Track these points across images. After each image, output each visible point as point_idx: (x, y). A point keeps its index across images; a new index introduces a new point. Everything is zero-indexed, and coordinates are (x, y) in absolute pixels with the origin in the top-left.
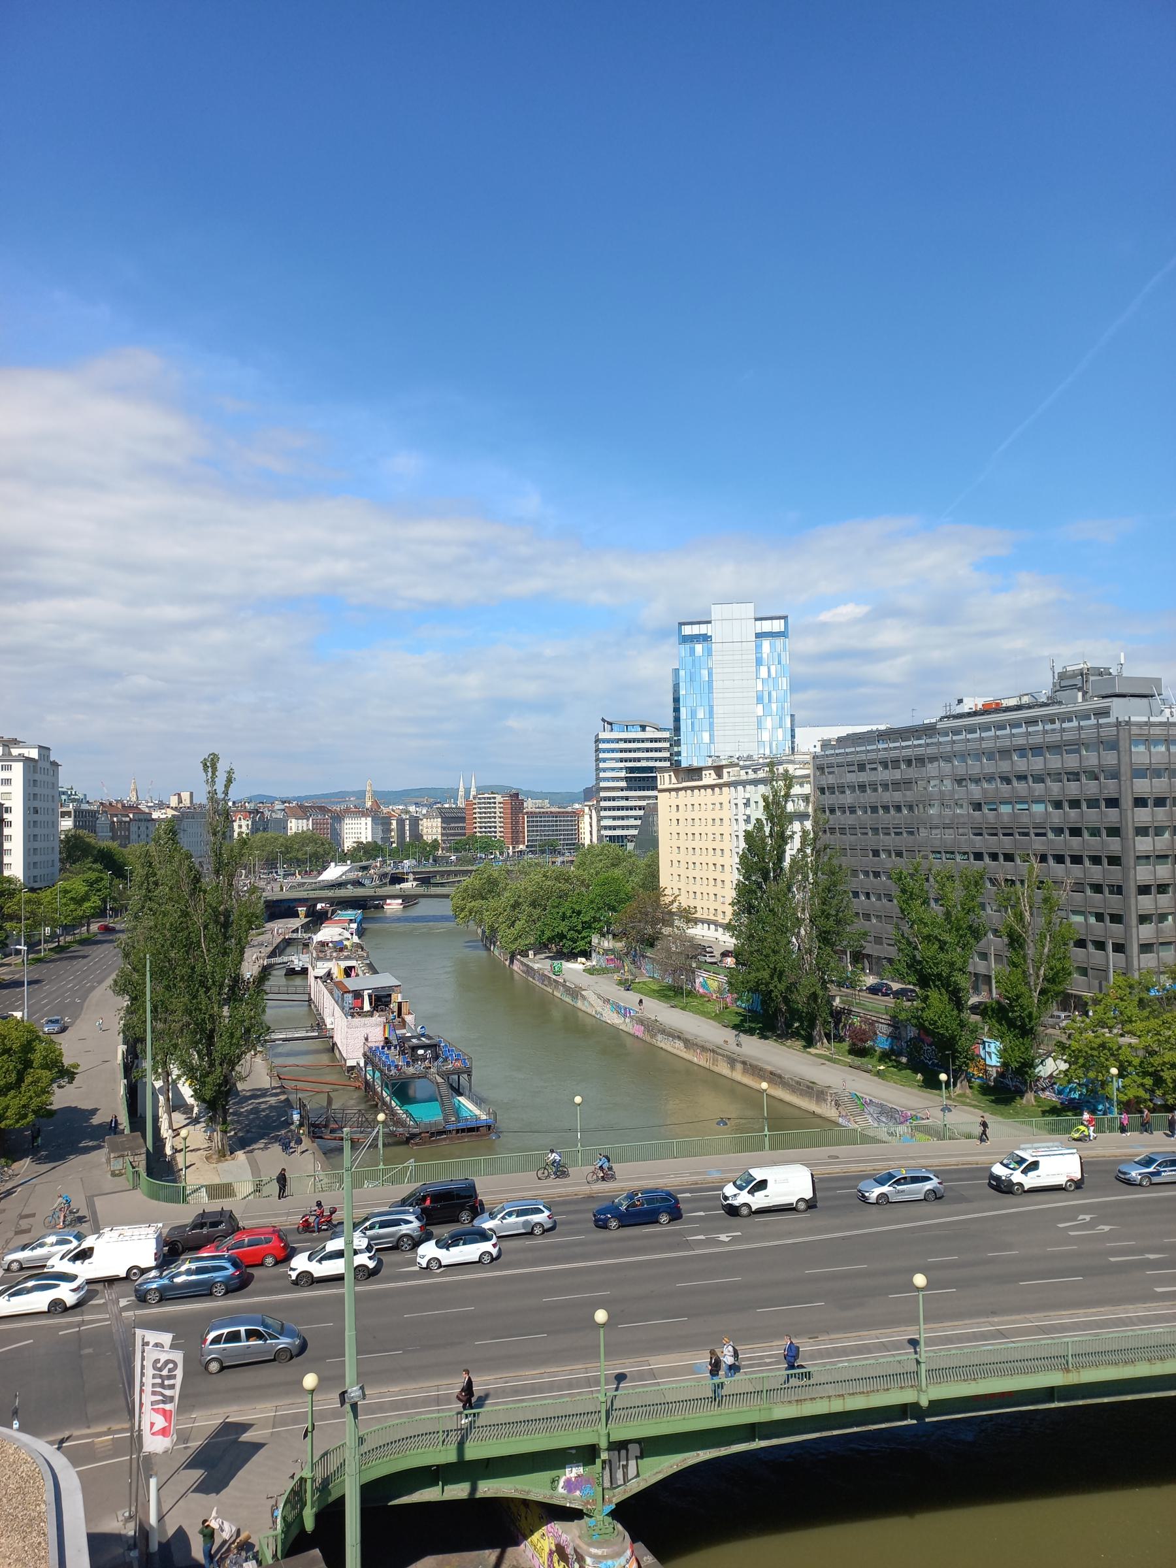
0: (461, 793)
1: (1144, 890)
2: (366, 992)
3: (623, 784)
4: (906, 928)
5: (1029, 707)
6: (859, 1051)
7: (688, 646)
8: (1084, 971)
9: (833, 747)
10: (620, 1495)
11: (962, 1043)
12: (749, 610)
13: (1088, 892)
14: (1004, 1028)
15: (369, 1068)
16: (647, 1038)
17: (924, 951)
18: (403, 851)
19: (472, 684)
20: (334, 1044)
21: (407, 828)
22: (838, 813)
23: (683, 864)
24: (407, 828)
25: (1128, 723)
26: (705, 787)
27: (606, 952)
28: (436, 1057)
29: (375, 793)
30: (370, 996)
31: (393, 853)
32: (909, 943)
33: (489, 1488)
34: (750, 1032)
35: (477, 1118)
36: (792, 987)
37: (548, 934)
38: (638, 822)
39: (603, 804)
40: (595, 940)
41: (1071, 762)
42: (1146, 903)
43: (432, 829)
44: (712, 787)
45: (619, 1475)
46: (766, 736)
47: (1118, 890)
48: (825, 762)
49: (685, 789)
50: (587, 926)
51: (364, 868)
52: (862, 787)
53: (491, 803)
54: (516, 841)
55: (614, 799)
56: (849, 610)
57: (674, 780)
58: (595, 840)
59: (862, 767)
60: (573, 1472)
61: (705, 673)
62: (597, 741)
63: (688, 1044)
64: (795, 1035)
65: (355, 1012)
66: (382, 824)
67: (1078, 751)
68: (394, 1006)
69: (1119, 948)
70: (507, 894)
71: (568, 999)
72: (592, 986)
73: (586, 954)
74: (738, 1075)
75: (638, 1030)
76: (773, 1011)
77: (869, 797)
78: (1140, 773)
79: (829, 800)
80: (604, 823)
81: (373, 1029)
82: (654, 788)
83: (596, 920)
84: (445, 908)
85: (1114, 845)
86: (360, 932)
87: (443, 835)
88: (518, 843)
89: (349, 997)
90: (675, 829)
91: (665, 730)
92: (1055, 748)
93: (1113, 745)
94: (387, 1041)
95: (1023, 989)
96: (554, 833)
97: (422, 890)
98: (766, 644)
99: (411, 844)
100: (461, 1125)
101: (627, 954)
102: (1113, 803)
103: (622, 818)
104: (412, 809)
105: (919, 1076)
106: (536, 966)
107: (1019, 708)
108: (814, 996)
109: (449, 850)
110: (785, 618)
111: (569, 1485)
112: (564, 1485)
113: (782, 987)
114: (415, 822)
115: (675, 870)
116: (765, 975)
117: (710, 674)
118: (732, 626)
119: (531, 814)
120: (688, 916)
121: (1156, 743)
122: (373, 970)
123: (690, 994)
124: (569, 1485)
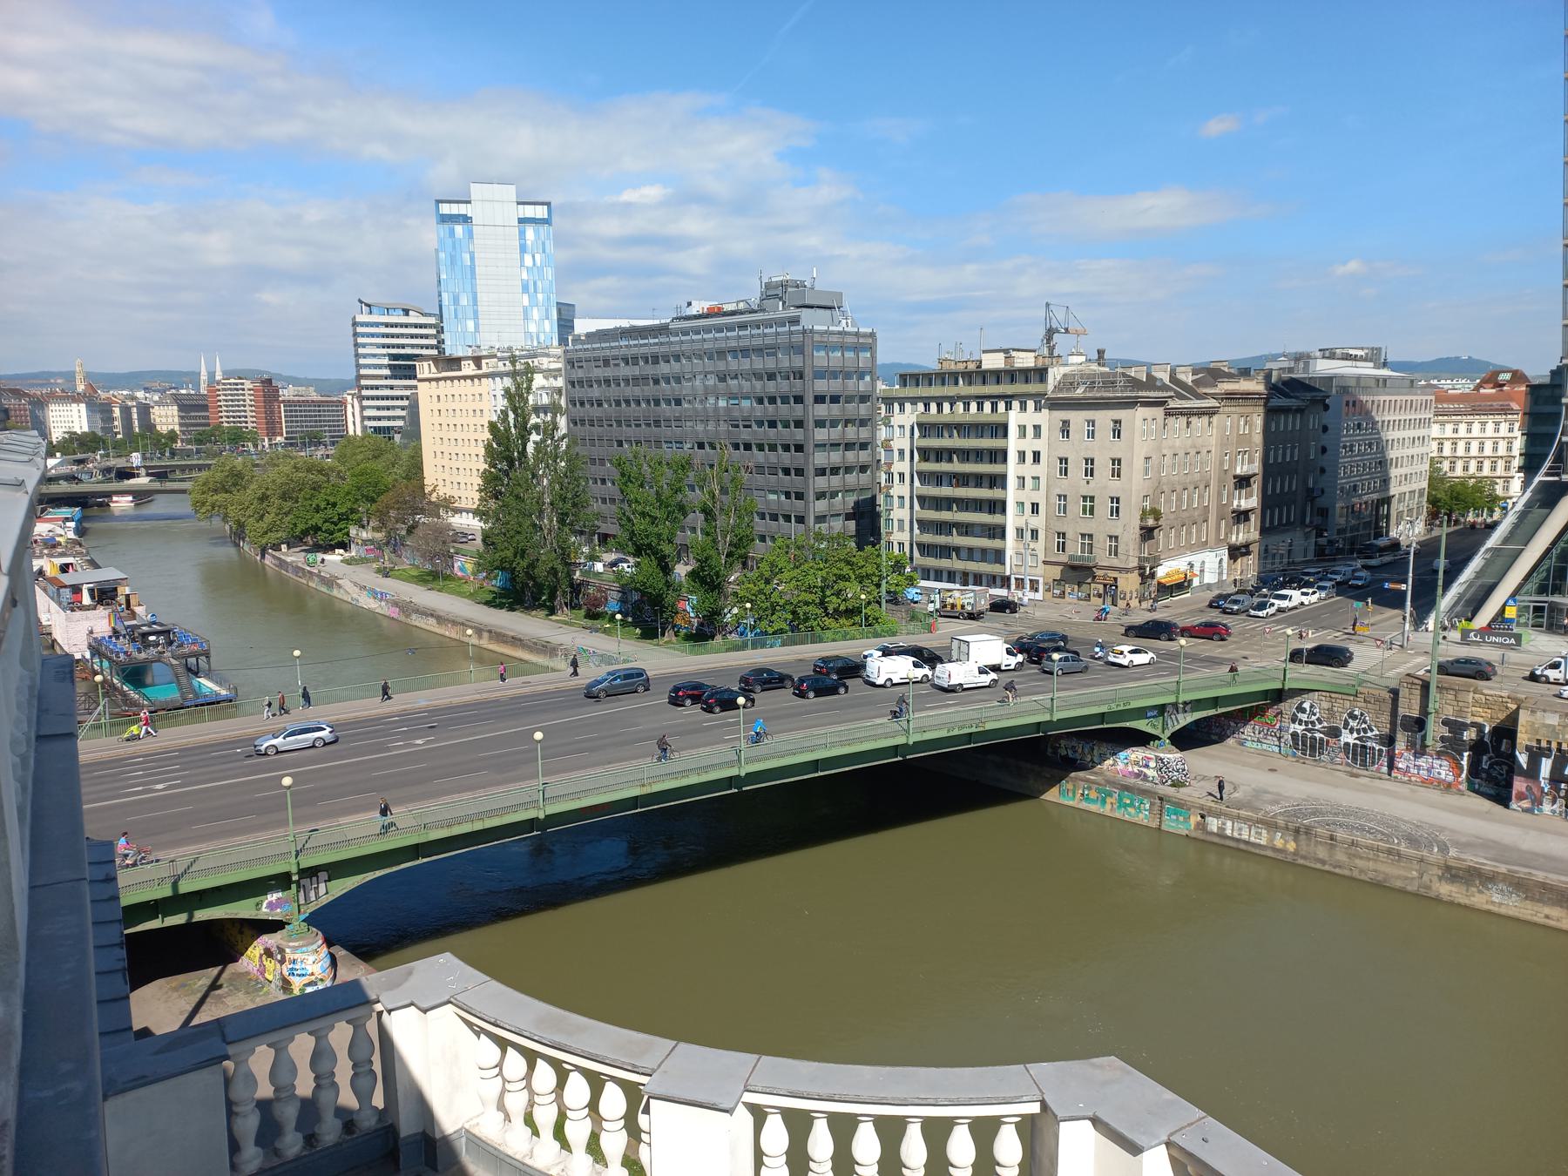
0: (204, 377)
1: (821, 472)
2: (85, 587)
3: (387, 372)
4: (626, 506)
5: (741, 313)
6: (592, 616)
7: (446, 226)
8: (763, 539)
9: (583, 343)
10: (312, 908)
11: (669, 599)
12: (510, 192)
13: (781, 475)
14: (697, 585)
15: (96, 660)
16: (402, 618)
17: (640, 525)
18: (131, 442)
19: (217, 248)
20: (54, 641)
21: (135, 416)
22: (664, 405)
23: (446, 455)
24: (135, 416)
25: (812, 331)
26: (465, 378)
27: (365, 542)
28: (170, 643)
29: (88, 376)
30: (91, 591)
31: (117, 445)
32: (629, 520)
33: (201, 915)
34: (500, 606)
35: (217, 694)
36: (532, 565)
37: (301, 527)
38: (403, 413)
39: (365, 393)
40: (353, 531)
41: (770, 363)
42: (821, 483)
43: (166, 418)
44: (472, 378)
45: (312, 894)
46: (533, 328)
47: (800, 472)
48: (575, 356)
49: (445, 379)
50: (344, 518)
51: (80, 462)
52: (607, 381)
53: (237, 388)
54: (272, 431)
55: (377, 388)
56: (652, 193)
57: (434, 369)
58: (359, 433)
59: (606, 362)
60: (273, 897)
61: (467, 257)
62: (355, 324)
63: (440, 619)
64: (542, 606)
65: (75, 606)
66: (102, 412)
67: (775, 354)
68: (121, 599)
69: (801, 520)
70: (253, 486)
71: (324, 589)
72: (351, 577)
73: (344, 546)
74: (485, 642)
75: (394, 612)
76: (524, 586)
77: (613, 392)
78: (820, 374)
79: (579, 393)
80: (367, 413)
81: (100, 622)
82: (415, 377)
83: (353, 511)
84: (183, 506)
85: (799, 435)
86: (80, 531)
87: (181, 425)
88: (274, 434)
89: (66, 593)
90: (437, 420)
91: (430, 315)
92: (759, 351)
93: (800, 350)
94: (116, 634)
95: (713, 553)
96: (316, 423)
97: (157, 485)
98: (530, 232)
99: (142, 436)
100: (200, 701)
101: (387, 544)
102: (799, 399)
103: (388, 408)
104: (140, 394)
105: (638, 631)
106: (289, 559)
107: (733, 313)
108: (554, 572)
109: (189, 442)
110: (548, 204)
111: (270, 905)
112: (267, 906)
113: (524, 564)
114: (145, 410)
115: (439, 462)
116: (509, 554)
117: (472, 259)
118: (494, 208)
119: (288, 403)
120: (448, 504)
121: (834, 349)
122: (94, 565)
123: (447, 578)
124: (270, 905)
